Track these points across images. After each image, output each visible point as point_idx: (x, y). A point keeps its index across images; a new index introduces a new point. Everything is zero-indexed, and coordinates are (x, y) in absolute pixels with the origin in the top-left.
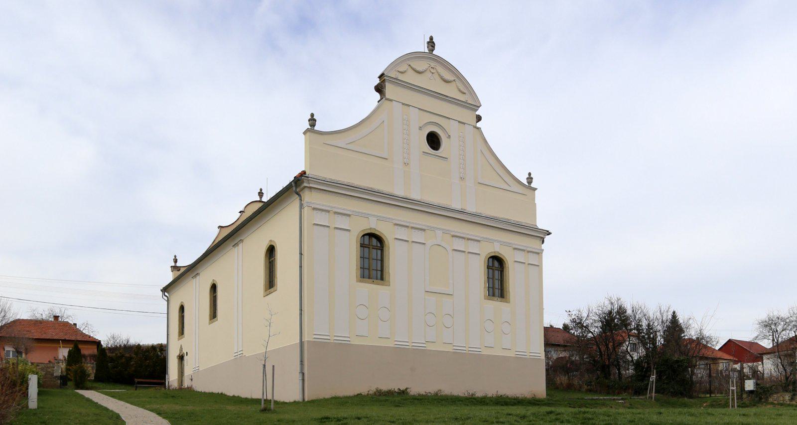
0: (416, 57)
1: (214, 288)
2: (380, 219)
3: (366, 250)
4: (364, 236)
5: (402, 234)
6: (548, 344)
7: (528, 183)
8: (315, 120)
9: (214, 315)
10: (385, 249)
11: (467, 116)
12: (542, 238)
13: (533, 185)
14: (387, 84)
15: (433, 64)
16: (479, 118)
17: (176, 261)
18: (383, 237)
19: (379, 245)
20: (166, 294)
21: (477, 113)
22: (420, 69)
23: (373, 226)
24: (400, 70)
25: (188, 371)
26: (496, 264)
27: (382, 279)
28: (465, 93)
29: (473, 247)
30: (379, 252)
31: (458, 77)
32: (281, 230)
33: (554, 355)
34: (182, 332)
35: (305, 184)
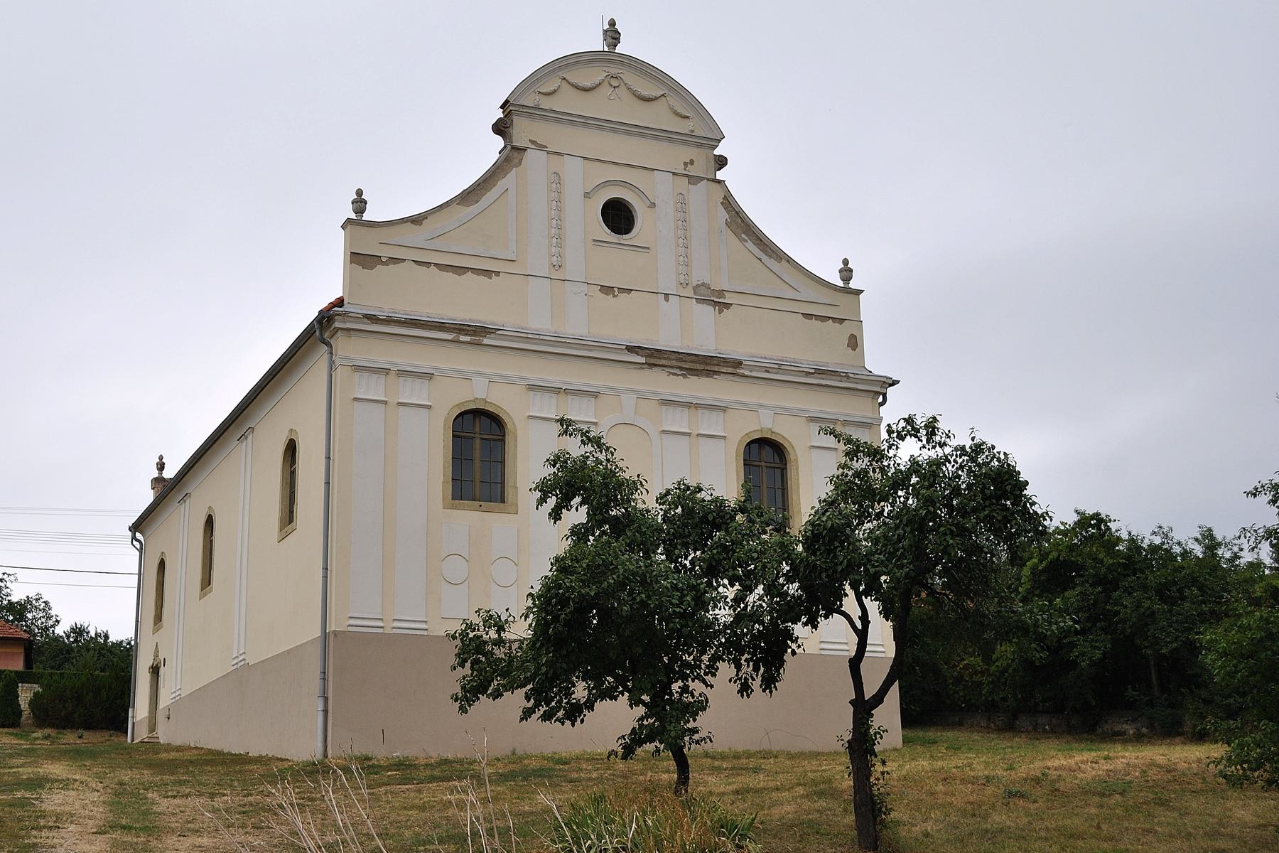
1: (210, 522)
2: (493, 380)
9: (207, 581)
14: (515, 118)
16: (722, 162)
17: (161, 467)
20: (138, 535)
21: (717, 152)
22: (588, 84)
23: (481, 395)
29: (710, 424)
32: (301, 411)
34: (158, 618)
35: (337, 325)
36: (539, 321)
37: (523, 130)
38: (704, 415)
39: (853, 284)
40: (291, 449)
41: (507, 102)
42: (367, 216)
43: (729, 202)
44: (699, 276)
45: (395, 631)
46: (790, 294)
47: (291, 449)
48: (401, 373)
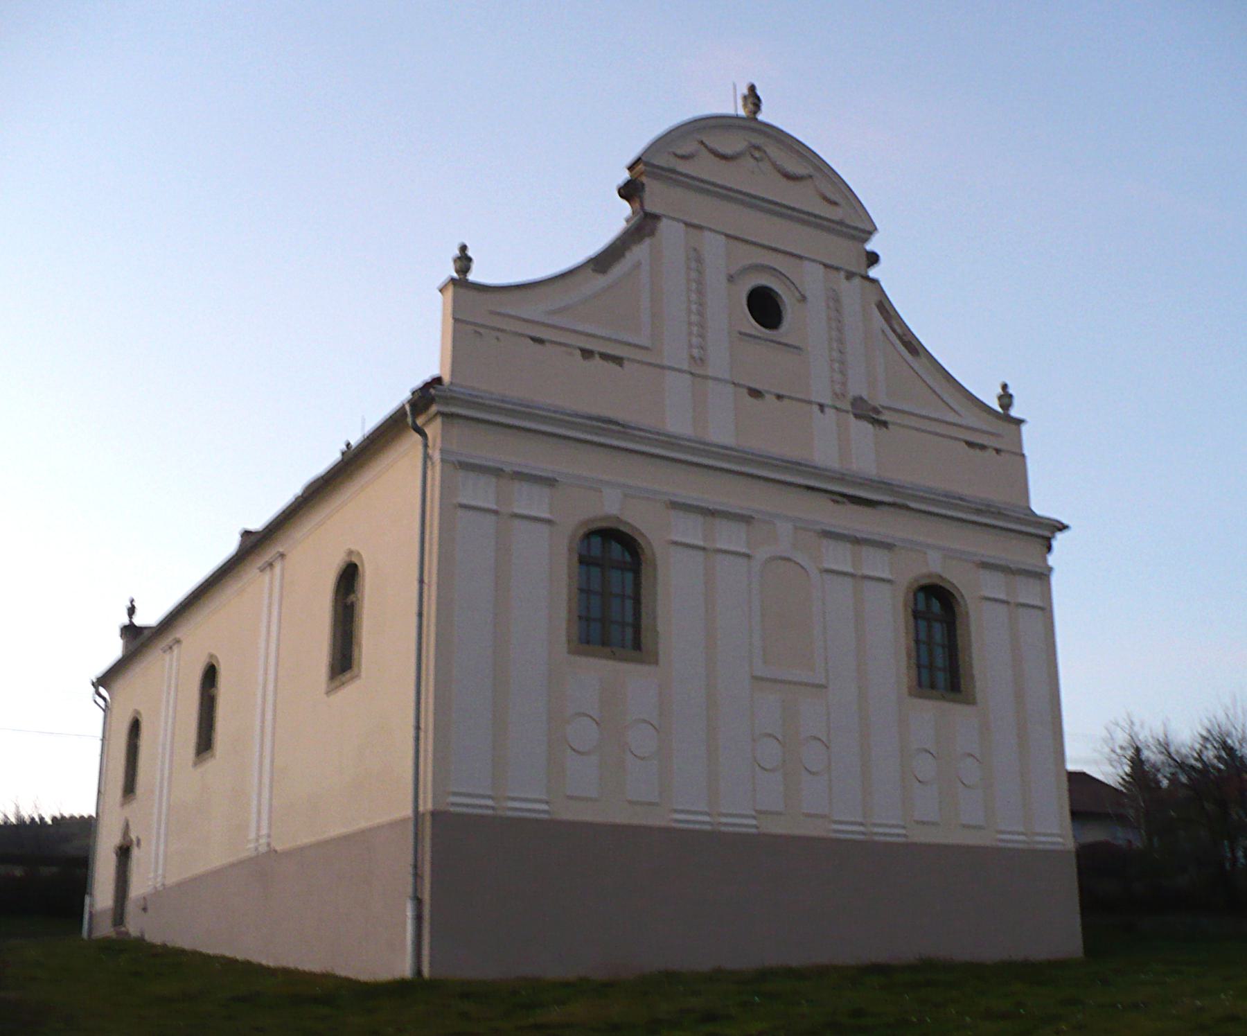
0: (714, 127)
1: (210, 675)
3: (595, 571)
4: (589, 535)
5: (689, 530)
6: (1078, 815)
7: (1001, 406)
8: (470, 260)
9: (205, 743)
10: (645, 570)
11: (840, 251)
12: (1043, 537)
13: (1014, 412)
15: (758, 140)
16: (873, 259)
17: (131, 611)
18: (640, 541)
19: (628, 558)
20: (102, 690)
21: (869, 247)
22: (728, 151)
24: (679, 152)
25: (139, 887)
26: (936, 608)
27: (637, 645)
28: (835, 203)
29: (876, 564)
30: (629, 576)
31: (818, 169)
33: (1096, 834)
36: (678, 423)
37: (657, 196)
38: (866, 551)
39: (1014, 412)
40: (349, 577)
41: (638, 161)
42: (472, 277)
43: (885, 308)
44: (857, 388)
45: (510, 814)
46: (951, 417)
47: (349, 577)
48: (519, 476)
